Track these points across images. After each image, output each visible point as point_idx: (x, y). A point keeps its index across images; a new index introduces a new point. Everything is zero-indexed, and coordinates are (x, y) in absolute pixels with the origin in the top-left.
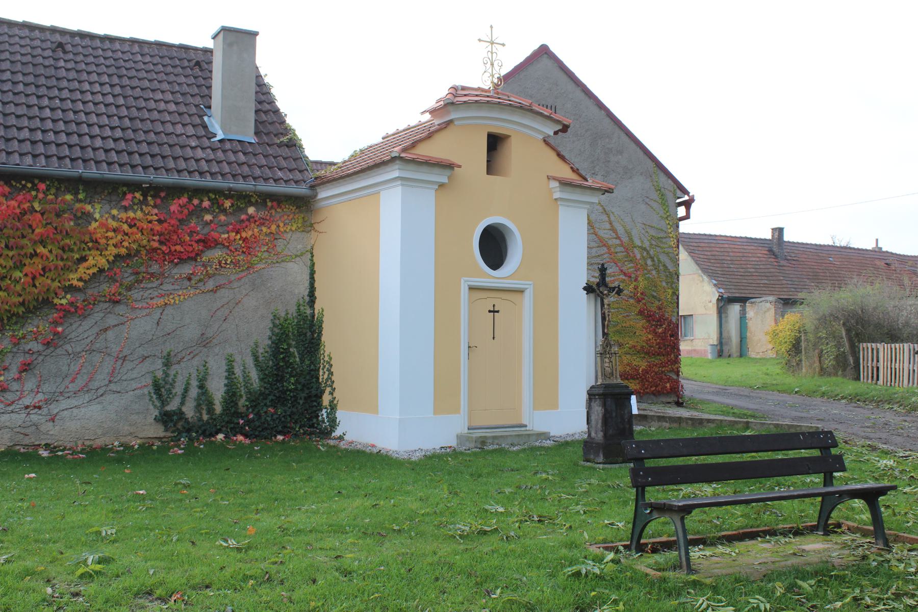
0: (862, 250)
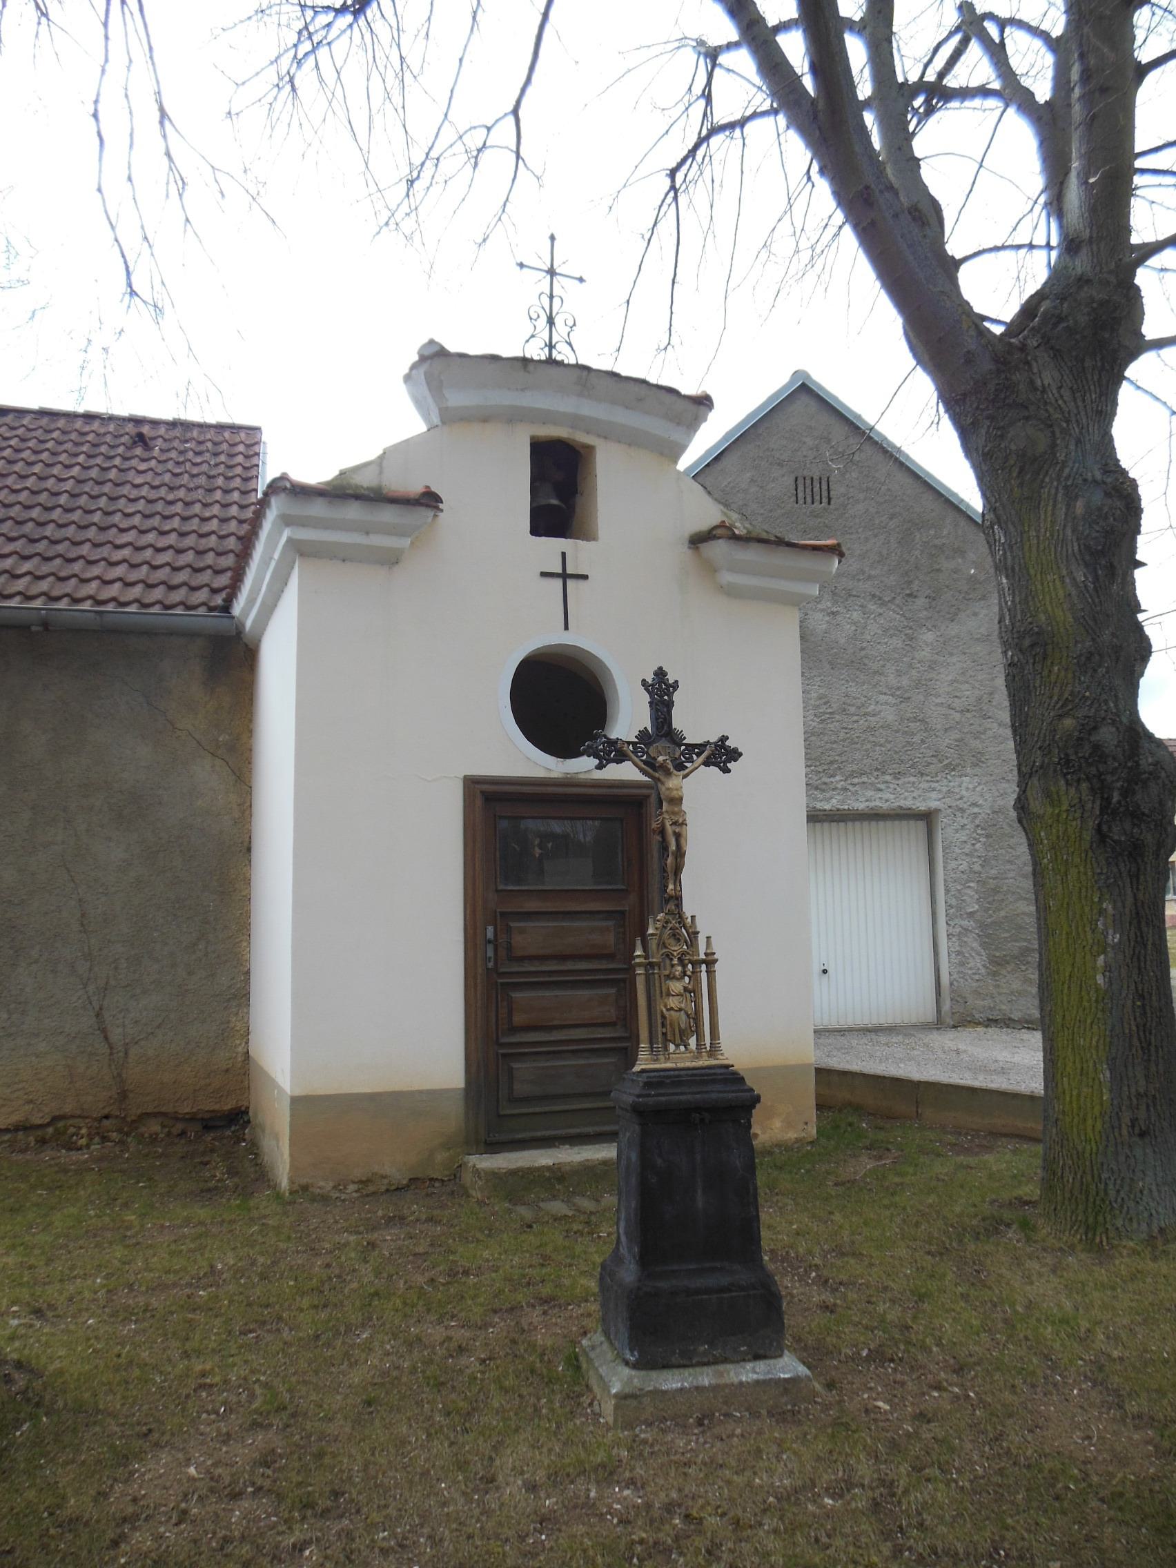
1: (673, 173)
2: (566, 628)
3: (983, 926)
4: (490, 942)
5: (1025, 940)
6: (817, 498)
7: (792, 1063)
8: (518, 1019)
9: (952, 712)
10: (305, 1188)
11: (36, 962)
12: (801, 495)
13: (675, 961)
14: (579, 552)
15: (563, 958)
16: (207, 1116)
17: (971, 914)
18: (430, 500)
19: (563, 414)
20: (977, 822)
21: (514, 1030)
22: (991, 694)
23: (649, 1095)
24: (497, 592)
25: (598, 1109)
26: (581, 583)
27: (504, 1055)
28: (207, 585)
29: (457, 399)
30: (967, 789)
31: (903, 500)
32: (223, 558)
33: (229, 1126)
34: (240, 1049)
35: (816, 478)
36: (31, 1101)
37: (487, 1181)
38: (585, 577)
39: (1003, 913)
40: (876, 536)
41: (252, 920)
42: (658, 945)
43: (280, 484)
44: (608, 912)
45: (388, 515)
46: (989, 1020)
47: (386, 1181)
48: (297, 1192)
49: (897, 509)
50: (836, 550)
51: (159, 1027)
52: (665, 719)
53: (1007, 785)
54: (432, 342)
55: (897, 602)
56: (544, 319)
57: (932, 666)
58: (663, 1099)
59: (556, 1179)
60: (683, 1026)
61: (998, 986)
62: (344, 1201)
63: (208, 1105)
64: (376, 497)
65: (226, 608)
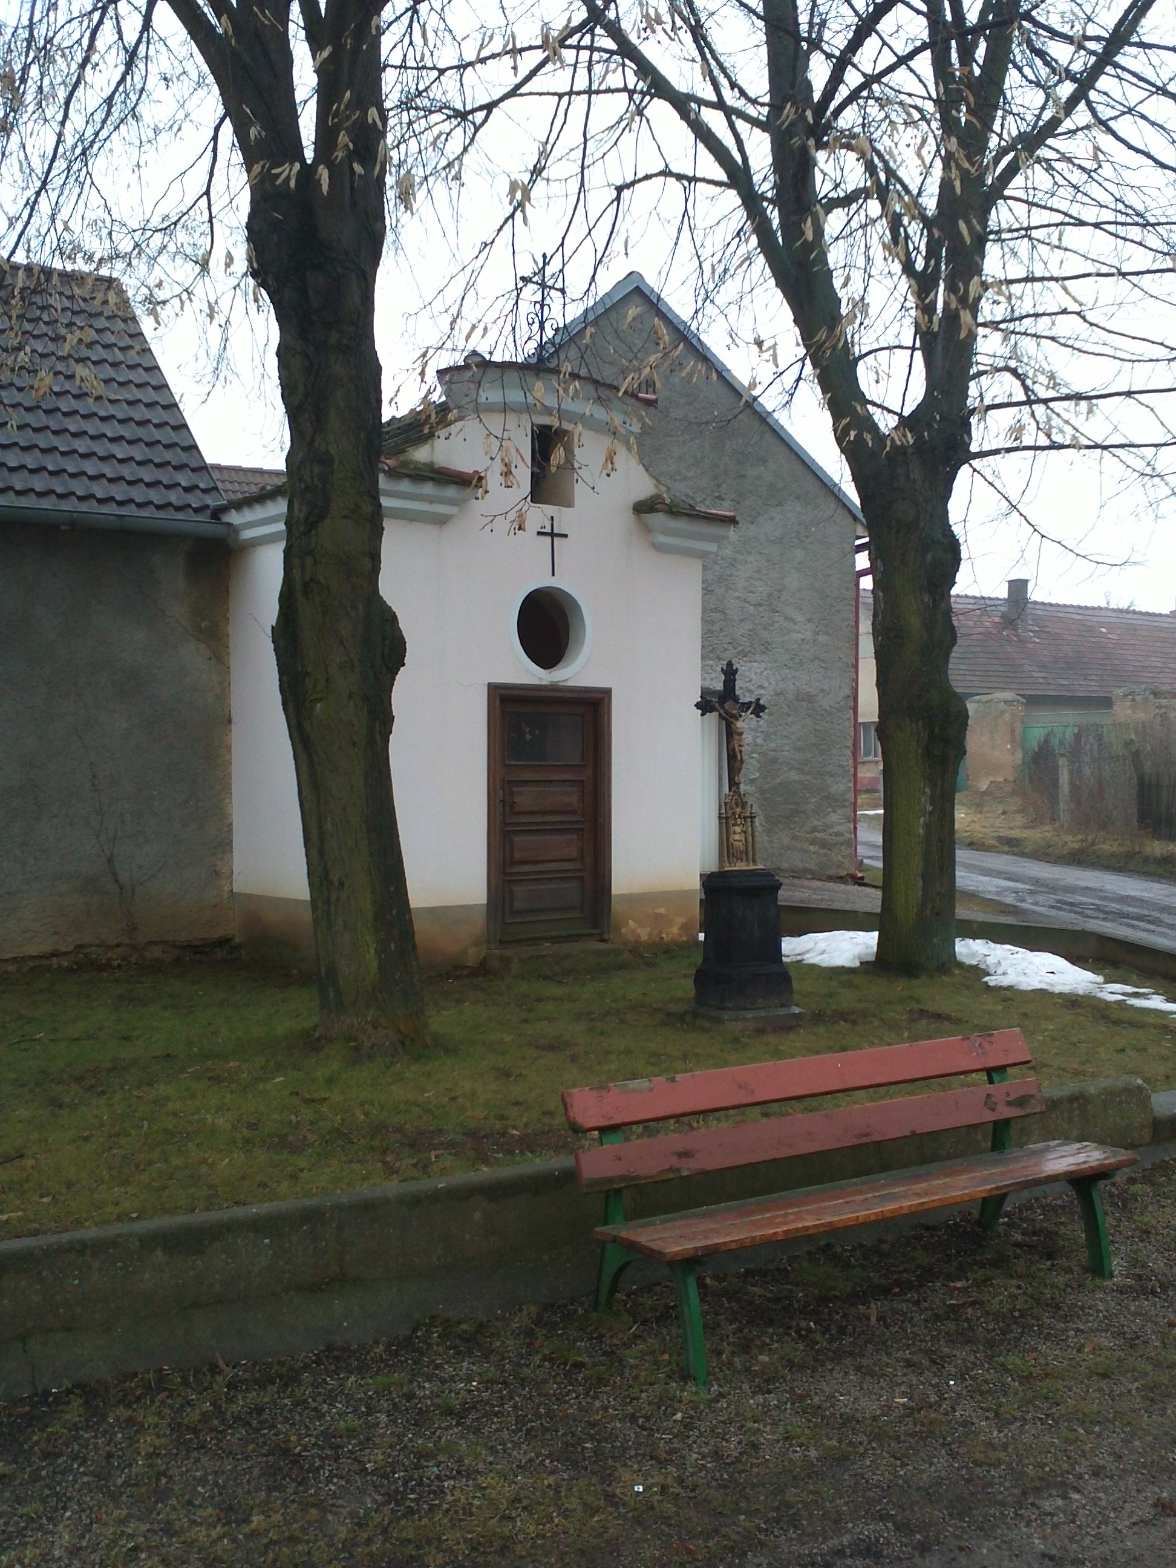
0: (1154, 615)
1: (620, 189)
2: (553, 574)
7: (686, 888)
8: (517, 856)
11: (56, 816)
14: (564, 518)
15: (545, 813)
21: (514, 863)
26: (563, 539)
27: (509, 881)
30: (756, 673)
36: (57, 933)
38: (566, 536)
40: (692, 440)
51: (160, 870)
53: (787, 671)
55: (707, 503)
57: (733, 563)
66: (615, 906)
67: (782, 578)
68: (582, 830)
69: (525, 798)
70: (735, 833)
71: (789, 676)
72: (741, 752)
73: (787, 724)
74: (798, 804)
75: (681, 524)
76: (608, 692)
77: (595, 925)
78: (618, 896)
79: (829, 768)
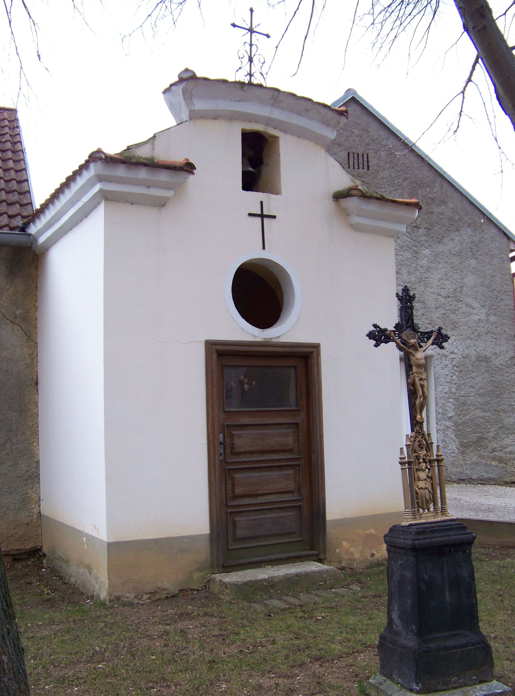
2: (264, 248)
3: (457, 425)
4: (221, 443)
5: (480, 432)
6: (361, 166)
7: (393, 511)
8: (238, 490)
9: (440, 297)
10: (118, 598)
12: (351, 164)
13: (421, 460)
14: (272, 203)
15: (263, 452)
16: (16, 553)
17: (450, 418)
18: (189, 168)
19: (261, 116)
20: (454, 363)
21: (235, 497)
22: (462, 287)
23: (420, 539)
24: (219, 227)
25: (278, 544)
26: (272, 220)
27: (230, 513)
28: (6, 213)
29: (199, 105)
31: (411, 170)
32: (11, 195)
33: (28, 558)
34: (35, 510)
35: (360, 154)
37: (232, 589)
38: (274, 217)
39: (468, 417)
40: (395, 190)
41: (40, 428)
42: (412, 450)
43: (98, 155)
44: (289, 424)
45: (164, 176)
46: (459, 479)
47: (165, 592)
48: (113, 600)
49: (408, 175)
50: (417, 206)
52: (409, 317)
54: (187, 70)
56: (247, 58)
58: (428, 541)
59: (269, 586)
60: (428, 498)
61: (465, 460)
62: (142, 605)
63: (16, 546)
64: (152, 165)
65: (23, 229)
66: (330, 530)
67: (462, 279)
68: (298, 465)
69: (245, 440)
70: (419, 480)
71: (472, 345)
72: (422, 386)
73: (472, 378)
74: (482, 433)
75: (372, 207)
76: (316, 347)
77: (312, 548)
78: (331, 521)
79: (503, 407)
